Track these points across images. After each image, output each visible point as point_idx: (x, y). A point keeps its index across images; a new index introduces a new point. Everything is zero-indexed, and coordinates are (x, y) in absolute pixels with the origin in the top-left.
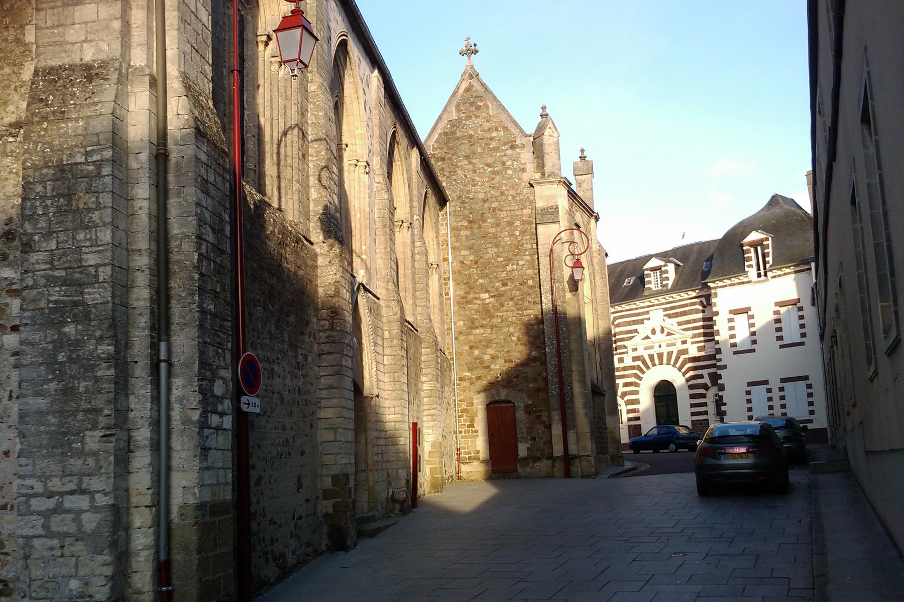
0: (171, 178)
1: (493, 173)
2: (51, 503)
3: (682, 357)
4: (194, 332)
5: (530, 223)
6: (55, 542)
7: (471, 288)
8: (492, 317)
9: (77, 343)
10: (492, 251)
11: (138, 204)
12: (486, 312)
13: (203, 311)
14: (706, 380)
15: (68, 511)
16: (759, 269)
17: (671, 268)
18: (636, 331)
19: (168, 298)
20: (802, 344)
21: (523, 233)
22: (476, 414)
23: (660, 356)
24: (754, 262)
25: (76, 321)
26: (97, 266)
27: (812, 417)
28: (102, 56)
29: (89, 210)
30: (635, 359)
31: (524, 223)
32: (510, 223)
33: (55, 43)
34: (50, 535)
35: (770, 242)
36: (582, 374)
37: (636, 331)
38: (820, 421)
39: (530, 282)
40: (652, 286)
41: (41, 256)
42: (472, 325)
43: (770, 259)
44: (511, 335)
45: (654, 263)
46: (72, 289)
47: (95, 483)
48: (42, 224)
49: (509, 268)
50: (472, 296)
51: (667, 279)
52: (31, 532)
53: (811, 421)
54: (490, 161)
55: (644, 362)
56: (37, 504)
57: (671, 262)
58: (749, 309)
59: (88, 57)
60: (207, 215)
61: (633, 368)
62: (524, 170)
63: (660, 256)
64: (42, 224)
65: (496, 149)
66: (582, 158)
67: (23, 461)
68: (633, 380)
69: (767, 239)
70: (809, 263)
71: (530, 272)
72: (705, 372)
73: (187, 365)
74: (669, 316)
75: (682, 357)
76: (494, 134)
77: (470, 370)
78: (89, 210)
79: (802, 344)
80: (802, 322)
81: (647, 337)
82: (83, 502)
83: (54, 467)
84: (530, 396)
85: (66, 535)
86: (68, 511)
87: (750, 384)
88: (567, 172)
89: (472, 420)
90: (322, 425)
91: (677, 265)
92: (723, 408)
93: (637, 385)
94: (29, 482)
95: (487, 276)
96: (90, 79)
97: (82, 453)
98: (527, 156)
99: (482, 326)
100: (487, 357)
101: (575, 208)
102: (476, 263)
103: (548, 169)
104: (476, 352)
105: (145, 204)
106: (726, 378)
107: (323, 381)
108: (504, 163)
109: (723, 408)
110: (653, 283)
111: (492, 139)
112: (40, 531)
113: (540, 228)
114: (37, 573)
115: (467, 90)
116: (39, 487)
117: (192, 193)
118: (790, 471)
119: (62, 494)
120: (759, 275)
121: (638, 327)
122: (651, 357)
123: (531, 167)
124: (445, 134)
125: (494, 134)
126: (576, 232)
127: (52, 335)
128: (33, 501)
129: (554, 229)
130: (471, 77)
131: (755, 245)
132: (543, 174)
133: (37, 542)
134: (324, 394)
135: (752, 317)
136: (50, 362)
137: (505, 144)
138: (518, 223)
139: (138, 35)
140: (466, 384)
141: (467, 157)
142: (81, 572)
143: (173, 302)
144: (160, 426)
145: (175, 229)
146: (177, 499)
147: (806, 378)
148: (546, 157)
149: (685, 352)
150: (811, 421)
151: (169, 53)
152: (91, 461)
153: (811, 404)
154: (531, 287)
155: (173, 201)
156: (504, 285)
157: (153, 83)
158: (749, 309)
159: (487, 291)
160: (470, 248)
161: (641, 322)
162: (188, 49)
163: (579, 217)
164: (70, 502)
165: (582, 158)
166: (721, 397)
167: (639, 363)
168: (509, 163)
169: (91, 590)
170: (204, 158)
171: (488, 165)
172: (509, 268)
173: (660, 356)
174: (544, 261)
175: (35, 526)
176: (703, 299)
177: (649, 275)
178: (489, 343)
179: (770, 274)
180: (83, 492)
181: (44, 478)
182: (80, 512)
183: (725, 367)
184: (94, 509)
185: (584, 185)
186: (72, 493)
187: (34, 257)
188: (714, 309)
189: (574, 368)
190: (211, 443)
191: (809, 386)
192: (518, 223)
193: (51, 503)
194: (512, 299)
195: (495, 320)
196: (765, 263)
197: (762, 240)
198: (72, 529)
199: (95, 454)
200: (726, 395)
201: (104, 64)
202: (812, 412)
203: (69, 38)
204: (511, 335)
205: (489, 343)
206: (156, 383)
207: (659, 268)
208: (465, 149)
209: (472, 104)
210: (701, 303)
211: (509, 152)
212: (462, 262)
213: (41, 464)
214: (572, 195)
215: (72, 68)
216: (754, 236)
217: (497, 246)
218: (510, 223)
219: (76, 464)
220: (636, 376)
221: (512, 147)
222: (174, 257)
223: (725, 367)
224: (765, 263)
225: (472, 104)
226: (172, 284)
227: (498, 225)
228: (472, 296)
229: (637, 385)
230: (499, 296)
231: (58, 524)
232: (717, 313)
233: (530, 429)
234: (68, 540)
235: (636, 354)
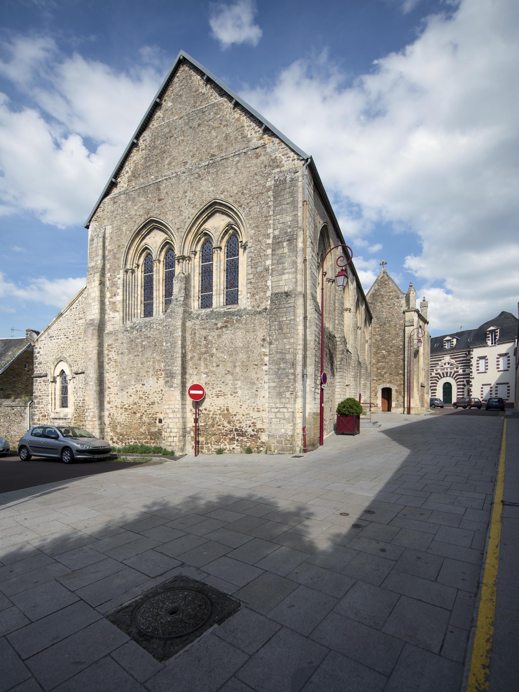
0: (308, 323)
1: (390, 308)
2: (277, 410)
3: (456, 374)
4: (313, 367)
5: (402, 326)
6: (278, 420)
7: (379, 349)
8: (385, 359)
9: (284, 369)
10: (387, 336)
11: (299, 331)
12: (384, 357)
13: (315, 361)
14: (465, 383)
15: (281, 412)
16: (492, 341)
17: (455, 340)
18: (438, 364)
19: (306, 357)
20: (508, 370)
21: (400, 329)
22: (378, 392)
23: (447, 373)
24: (490, 339)
25: (284, 363)
26: (289, 349)
27: (508, 398)
28: (290, 289)
29: (288, 333)
30: (436, 374)
31: (400, 325)
32: (395, 326)
33: (277, 286)
34: (277, 418)
35: (498, 331)
36: (418, 379)
37: (438, 364)
38: (511, 400)
39: (401, 347)
40: (446, 347)
41: (275, 346)
42: (378, 361)
43: (498, 337)
44: (393, 365)
45: (448, 338)
46: (282, 355)
47: (288, 406)
48: (275, 337)
49: (393, 342)
50: (379, 351)
51: (453, 344)
52: (272, 417)
53: (508, 400)
54: (389, 304)
55: (440, 375)
56: (273, 410)
57: (455, 338)
58: (486, 356)
59: (286, 290)
60: (317, 333)
61: (435, 377)
62: (402, 307)
63: (449, 335)
64: (275, 337)
65: (392, 299)
66: (424, 300)
67: (270, 399)
68: (435, 381)
69: (497, 329)
70: (515, 339)
71: (401, 343)
72: (465, 380)
73: (311, 376)
74: (452, 358)
75: (456, 374)
76: (391, 294)
77: (376, 377)
78: (288, 333)
79: (508, 370)
80: (509, 362)
81: (442, 366)
82: (285, 410)
83: (278, 401)
84: (397, 386)
85: (281, 418)
86: (281, 412)
87: (483, 385)
88: (418, 307)
89: (376, 394)
90: (336, 393)
91: (457, 339)
92: (471, 393)
93: (436, 383)
94: (271, 404)
95: (385, 344)
96: (287, 296)
97: (285, 398)
98: (403, 301)
99: (382, 362)
100: (383, 373)
101: (420, 320)
102: (381, 340)
103: (411, 306)
104: (379, 371)
105: (301, 331)
106: (473, 382)
107: (337, 380)
108: (394, 304)
109: (471, 393)
110: (447, 346)
111: (390, 295)
112: (274, 417)
113: (406, 328)
114: (273, 427)
115: (382, 278)
116: (274, 406)
117: (314, 328)
118: (214, 24)
119: (280, 408)
120: (492, 343)
121: (439, 363)
122: (443, 374)
123: (404, 305)
124: (373, 294)
125: (391, 294)
126: (420, 329)
127: (277, 367)
128: (272, 409)
129: (412, 328)
130: (384, 273)
131: (491, 332)
132: (409, 308)
133: (273, 420)
134: (337, 384)
135: (487, 363)
136: (276, 373)
137: (395, 297)
138: (398, 326)
139: (300, 282)
140: (374, 381)
141: (381, 302)
142: (285, 428)
143: (308, 359)
144: (304, 391)
145: (308, 338)
146: (308, 411)
147: (508, 383)
148: (411, 301)
149: (458, 372)
150: (508, 400)
151: (308, 287)
152: (287, 400)
153: (508, 393)
154: (401, 349)
155: (308, 330)
156: (391, 348)
157: (304, 297)
158: (486, 356)
159: (385, 350)
160: (380, 335)
161: (440, 360)
162: (312, 285)
163: (421, 323)
164: (281, 410)
165: (424, 300)
166: (471, 389)
167: (438, 376)
168: (396, 304)
169: (287, 432)
170: (316, 317)
171: (388, 305)
172: (393, 342)
173: (447, 373)
174: (407, 340)
175: (273, 415)
176: (467, 352)
177: (445, 343)
178: (384, 368)
179: (497, 343)
180: (285, 408)
181: (275, 403)
182: (284, 413)
183: (473, 378)
184: (288, 412)
185: (424, 311)
186: (282, 408)
187: (272, 346)
188: (471, 356)
189: (415, 377)
190: (316, 397)
191: (509, 387)
192: (398, 326)
193: (277, 410)
194: (394, 353)
195: (387, 360)
196: (495, 339)
197: (495, 330)
198: (282, 417)
199: (288, 398)
200: (472, 389)
201: (291, 292)
202: (508, 397)
203: (280, 284)
204: (393, 365)
205: (384, 368)
206: (303, 380)
207: (450, 340)
208: (380, 299)
209: (383, 283)
210: (466, 354)
211: (397, 300)
212: (376, 340)
213: (274, 400)
214: (420, 316)
215: (282, 293)
216: (492, 328)
217: (389, 334)
218: (395, 326)
219: (284, 400)
220: (436, 380)
221: (398, 298)
222: (308, 346)
223: (473, 378)
224: (495, 339)
225: (383, 283)
226: (307, 353)
227: (390, 326)
228: (379, 351)
229: (436, 383)
230: (389, 351)
231: (278, 415)
232: (472, 358)
233: (397, 398)
234: (281, 420)
235: (437, 372)
